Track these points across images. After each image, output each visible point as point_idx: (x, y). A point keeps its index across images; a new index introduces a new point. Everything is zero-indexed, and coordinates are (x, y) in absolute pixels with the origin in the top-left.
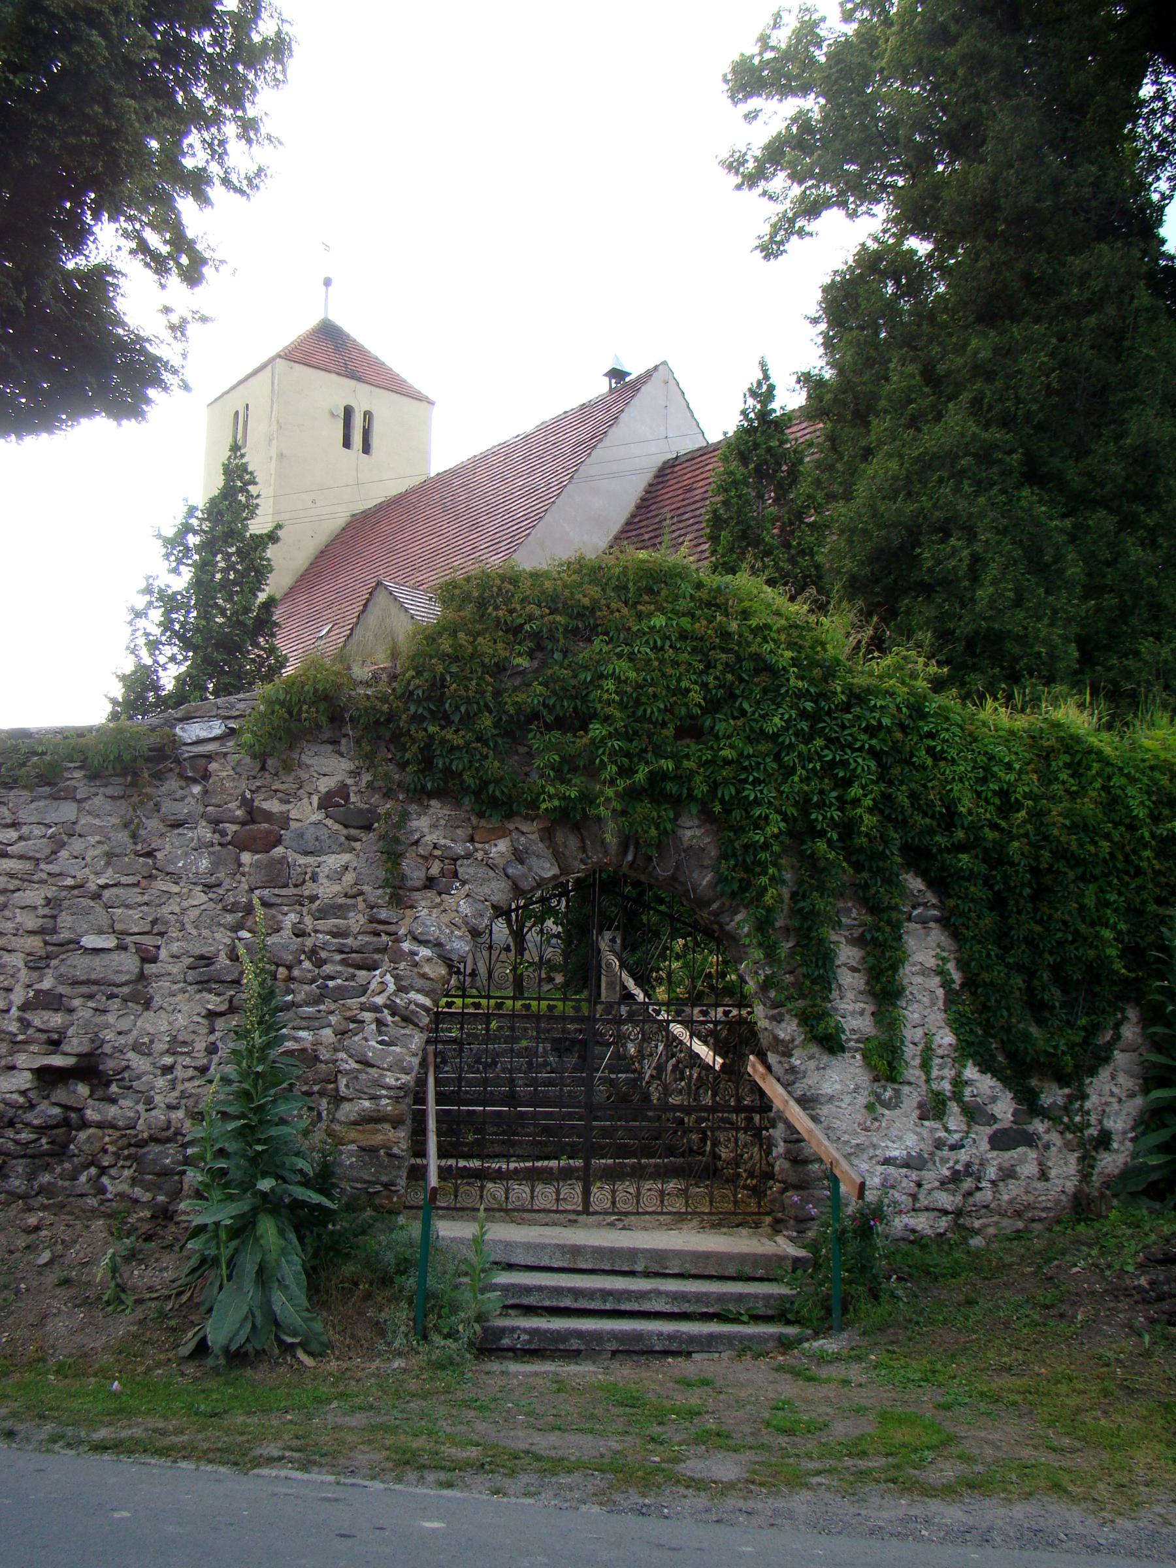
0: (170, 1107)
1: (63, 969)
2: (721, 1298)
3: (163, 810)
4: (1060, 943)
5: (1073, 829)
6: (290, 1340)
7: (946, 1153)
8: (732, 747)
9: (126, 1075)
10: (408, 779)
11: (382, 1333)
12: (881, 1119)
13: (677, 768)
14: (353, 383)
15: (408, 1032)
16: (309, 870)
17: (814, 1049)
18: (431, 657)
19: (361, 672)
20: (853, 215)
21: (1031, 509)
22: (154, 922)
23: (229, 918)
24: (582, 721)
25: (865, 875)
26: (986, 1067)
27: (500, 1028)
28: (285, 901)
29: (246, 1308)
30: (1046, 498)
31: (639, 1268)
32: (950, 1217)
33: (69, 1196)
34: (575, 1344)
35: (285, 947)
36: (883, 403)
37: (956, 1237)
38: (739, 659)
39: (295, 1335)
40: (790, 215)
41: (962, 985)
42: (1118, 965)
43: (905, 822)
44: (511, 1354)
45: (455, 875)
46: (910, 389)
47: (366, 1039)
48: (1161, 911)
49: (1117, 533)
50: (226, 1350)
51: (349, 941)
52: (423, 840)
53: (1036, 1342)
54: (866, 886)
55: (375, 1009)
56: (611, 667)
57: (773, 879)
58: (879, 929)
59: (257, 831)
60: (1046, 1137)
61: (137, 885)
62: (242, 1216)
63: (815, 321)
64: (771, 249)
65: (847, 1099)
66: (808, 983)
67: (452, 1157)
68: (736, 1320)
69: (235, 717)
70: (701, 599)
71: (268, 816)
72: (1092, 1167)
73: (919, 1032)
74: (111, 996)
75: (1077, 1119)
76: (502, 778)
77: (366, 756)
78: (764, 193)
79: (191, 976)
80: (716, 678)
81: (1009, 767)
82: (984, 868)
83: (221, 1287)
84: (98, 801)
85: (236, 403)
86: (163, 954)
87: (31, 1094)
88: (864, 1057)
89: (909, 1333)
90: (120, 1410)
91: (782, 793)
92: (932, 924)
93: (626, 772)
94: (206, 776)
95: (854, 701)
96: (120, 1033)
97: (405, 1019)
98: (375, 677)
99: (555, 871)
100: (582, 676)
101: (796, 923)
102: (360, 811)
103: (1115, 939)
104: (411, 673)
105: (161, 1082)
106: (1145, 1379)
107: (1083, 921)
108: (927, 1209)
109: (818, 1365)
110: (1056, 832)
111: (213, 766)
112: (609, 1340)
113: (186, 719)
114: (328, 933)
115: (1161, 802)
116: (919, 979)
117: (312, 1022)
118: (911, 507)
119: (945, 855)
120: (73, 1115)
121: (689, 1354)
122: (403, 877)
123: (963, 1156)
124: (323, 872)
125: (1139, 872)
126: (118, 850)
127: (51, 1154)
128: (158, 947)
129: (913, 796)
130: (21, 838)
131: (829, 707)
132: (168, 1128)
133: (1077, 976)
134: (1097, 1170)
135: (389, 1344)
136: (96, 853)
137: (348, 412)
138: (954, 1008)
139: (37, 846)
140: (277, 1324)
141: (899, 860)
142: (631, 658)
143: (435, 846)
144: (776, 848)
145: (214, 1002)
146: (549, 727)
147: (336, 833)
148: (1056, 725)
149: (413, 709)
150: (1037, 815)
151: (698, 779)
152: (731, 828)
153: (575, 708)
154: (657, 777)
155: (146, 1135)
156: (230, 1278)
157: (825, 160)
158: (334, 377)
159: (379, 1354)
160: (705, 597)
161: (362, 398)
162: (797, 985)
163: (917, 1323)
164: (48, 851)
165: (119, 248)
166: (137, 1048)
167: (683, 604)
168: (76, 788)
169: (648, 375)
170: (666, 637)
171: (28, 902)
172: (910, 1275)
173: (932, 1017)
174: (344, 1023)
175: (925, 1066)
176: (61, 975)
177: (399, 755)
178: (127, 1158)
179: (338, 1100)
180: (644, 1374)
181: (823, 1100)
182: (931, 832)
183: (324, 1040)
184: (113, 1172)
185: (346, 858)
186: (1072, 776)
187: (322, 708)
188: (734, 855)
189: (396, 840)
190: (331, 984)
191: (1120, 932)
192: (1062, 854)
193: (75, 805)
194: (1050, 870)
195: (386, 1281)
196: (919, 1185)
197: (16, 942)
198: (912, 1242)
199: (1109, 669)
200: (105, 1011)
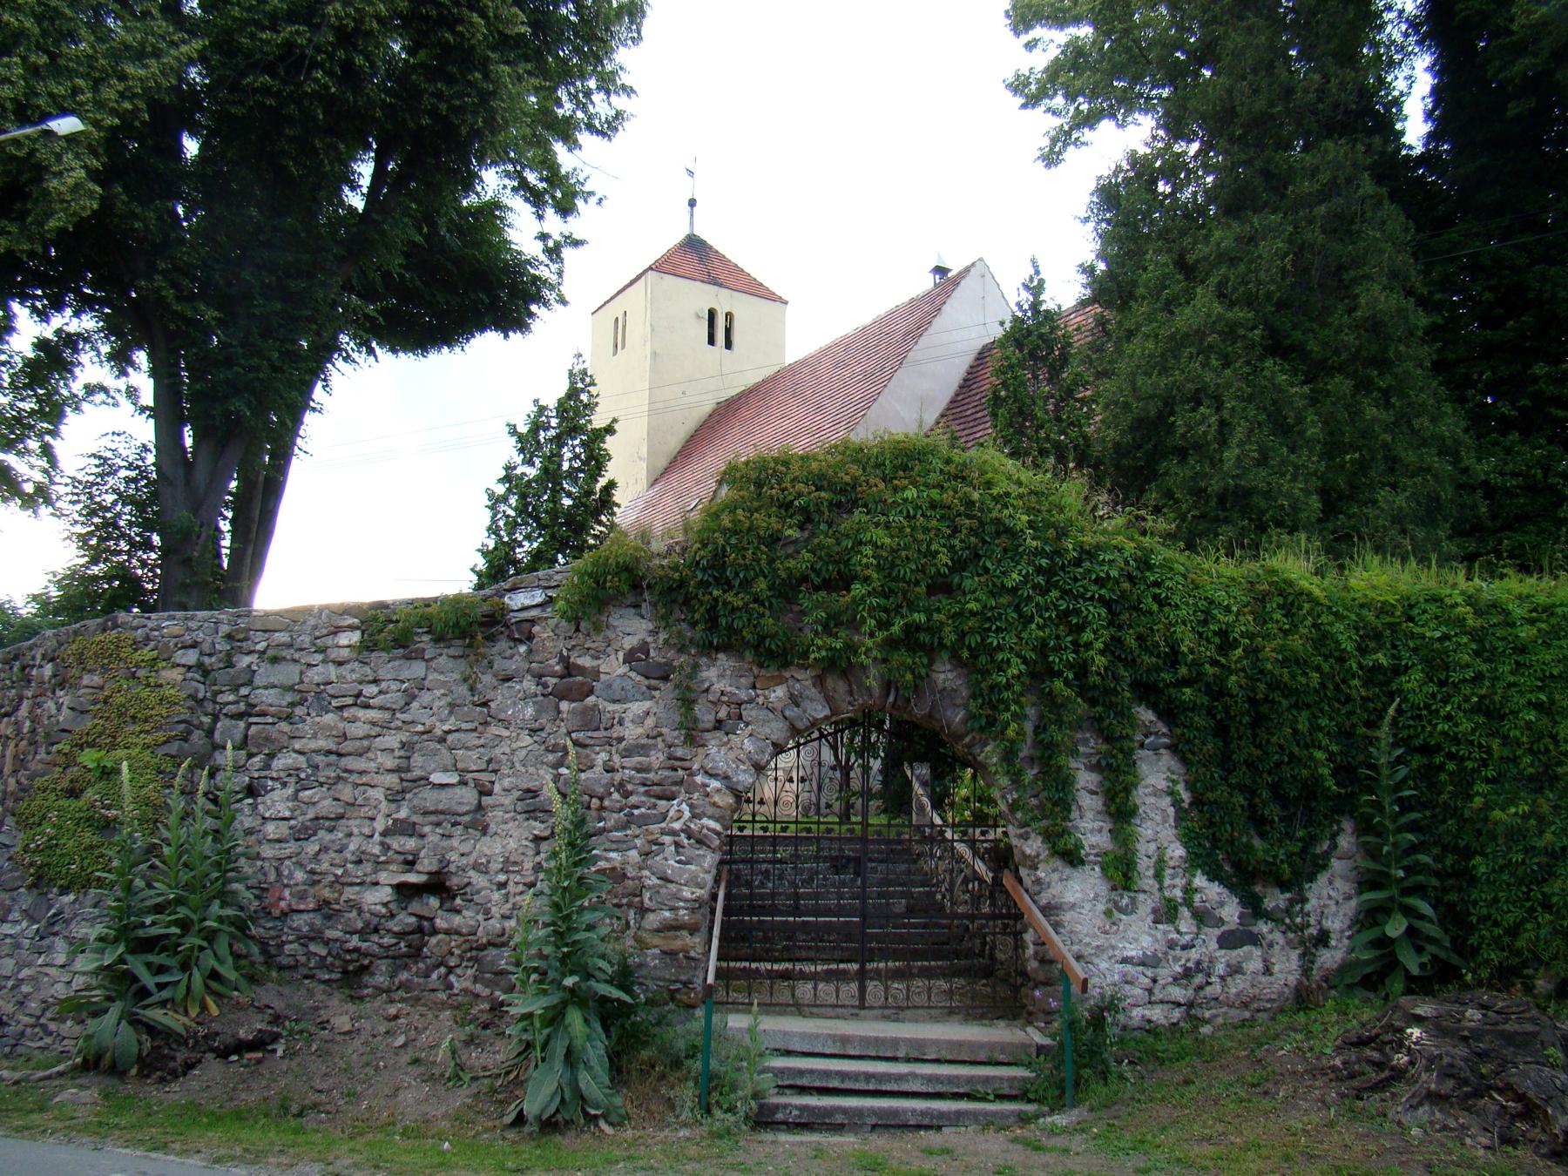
0: (504, 917)
1: (415, 802)
2: (970, 1080)
4: (1278, 765)
5: (1284, 663)
6: (593, 1112)
7: (1178, 952)
8: (977, 600)
10: (698, 636)
12: (1121, 921)
17: (1058, 863)
19: (657, 546)
20: (1121, 126)
21: (1273, 377)
22: (489, 762)
23: (551, 757)
24: (845, 582)
25: (1099, 709)
26: (1213, 876)
31: (901, 1054)
34: (839, 1119)
35: (598, 781)
36: (1141, 291)
38: (982, 524)
39: (597, 1108)
40: (1066, 128)
41: (1191, 804)
42: (1330, 783)
43: (1134, 661)
45: (740, 717)
46: (1165, 277)
48: (1369, 733)
49: (1353, 396)
50: (539, 1118)
51: (651, 775)
54: (1100, 719)
55: (674, 833)
57: (1015, 716)
58: (1114, 757)
59: (572, 683)
60: (1270, 937)
61: (475, 730)
62: (554, 1007)
64: (1051, 158)
65: (1088, 906)
66: (1049, 805)
68: (983, 1099)
71: (582, 670)
73: (1153, 846)
74: (454, 824)
75: (1298, 920)
77: (662, 618)
78: (1048, 110)
79: (520, 806)
81: (1228, 609)
82: (1205, 700)
86: (497, 788)
88: (1103, 869)
90: (441, 1164)
92: (1162, 751)
93: (883, 625)
94: (530, 637)
97: (699, 842)
98: (670, 549)
99: (827, 712)
100: (844, 544)
101: (1038, 753)
102: (659, 665)
104: (698, 545)
105: (496, 896)
106: (1325, 1146)
109: (1048, 1137)
110: (1269, 666)
111: (536, 629)
113: (513, 589)
115: (1368, 636)
116: (1152, 800)
117: (622, 846)
118: (1163, 381)
121: (939, 1128)
122: (696, 720)
123: (1194, 954)
124: (629, 716)
125: (1349, 699)
127: (409, 956)
128: (493, 783)
129: (1140, 638)
131: (1060, 566)
133: (1294, 793)
137: (712, 314)
140: (582, 1098)
141: (1128, 695)
142: (887, 526)
143: (722, 694)
144: (1017, 688)
145: (538, 828)
146: (817, 589)
148: (1273, 572)
150: (1253, 652)
151: (947, 629)
152: (979, 671)
153: (839, 572)
154: (911, 630)
156: (543, 1060)
158: (698, 284)
159: (669, 1125)
160: (953, 471)
161: (724, 301)
162: (1041, 807)
165: (505, 187)
166: (476, 867)
167: (934, 477)
169: (967, 270)
175: (1158, 876)
179: (643, 911)
180: (896, 1145)
182: (1158, 669)
184: (459, 971)
185: (647, 704)
186: (1285, 616)
188: (982, 695)
189: (688, 688)
190: (636, 812)
191: (1331, 754)
192: (1275, 685)
194: (1266, 700)
195: (677, 1064)
196: (1155, 981)
197: (378, 779)
199: (1350, 517)
200: (450, 836)
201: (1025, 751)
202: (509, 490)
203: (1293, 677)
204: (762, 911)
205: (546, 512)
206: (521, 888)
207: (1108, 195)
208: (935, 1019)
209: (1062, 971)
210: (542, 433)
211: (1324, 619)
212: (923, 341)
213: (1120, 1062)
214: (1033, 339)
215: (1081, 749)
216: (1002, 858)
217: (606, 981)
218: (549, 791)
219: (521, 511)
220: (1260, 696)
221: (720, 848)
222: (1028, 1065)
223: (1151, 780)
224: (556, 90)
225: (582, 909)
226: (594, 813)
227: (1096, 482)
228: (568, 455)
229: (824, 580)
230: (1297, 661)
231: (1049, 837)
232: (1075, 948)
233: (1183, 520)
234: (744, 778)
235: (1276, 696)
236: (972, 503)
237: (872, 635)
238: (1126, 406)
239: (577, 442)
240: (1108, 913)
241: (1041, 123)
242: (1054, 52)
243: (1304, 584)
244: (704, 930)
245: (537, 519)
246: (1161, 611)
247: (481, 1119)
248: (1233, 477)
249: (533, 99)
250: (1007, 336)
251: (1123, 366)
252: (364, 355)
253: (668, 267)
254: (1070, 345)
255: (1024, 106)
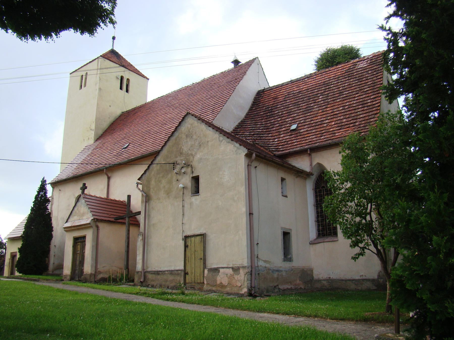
137: (122, 78)
161: (127, 74)
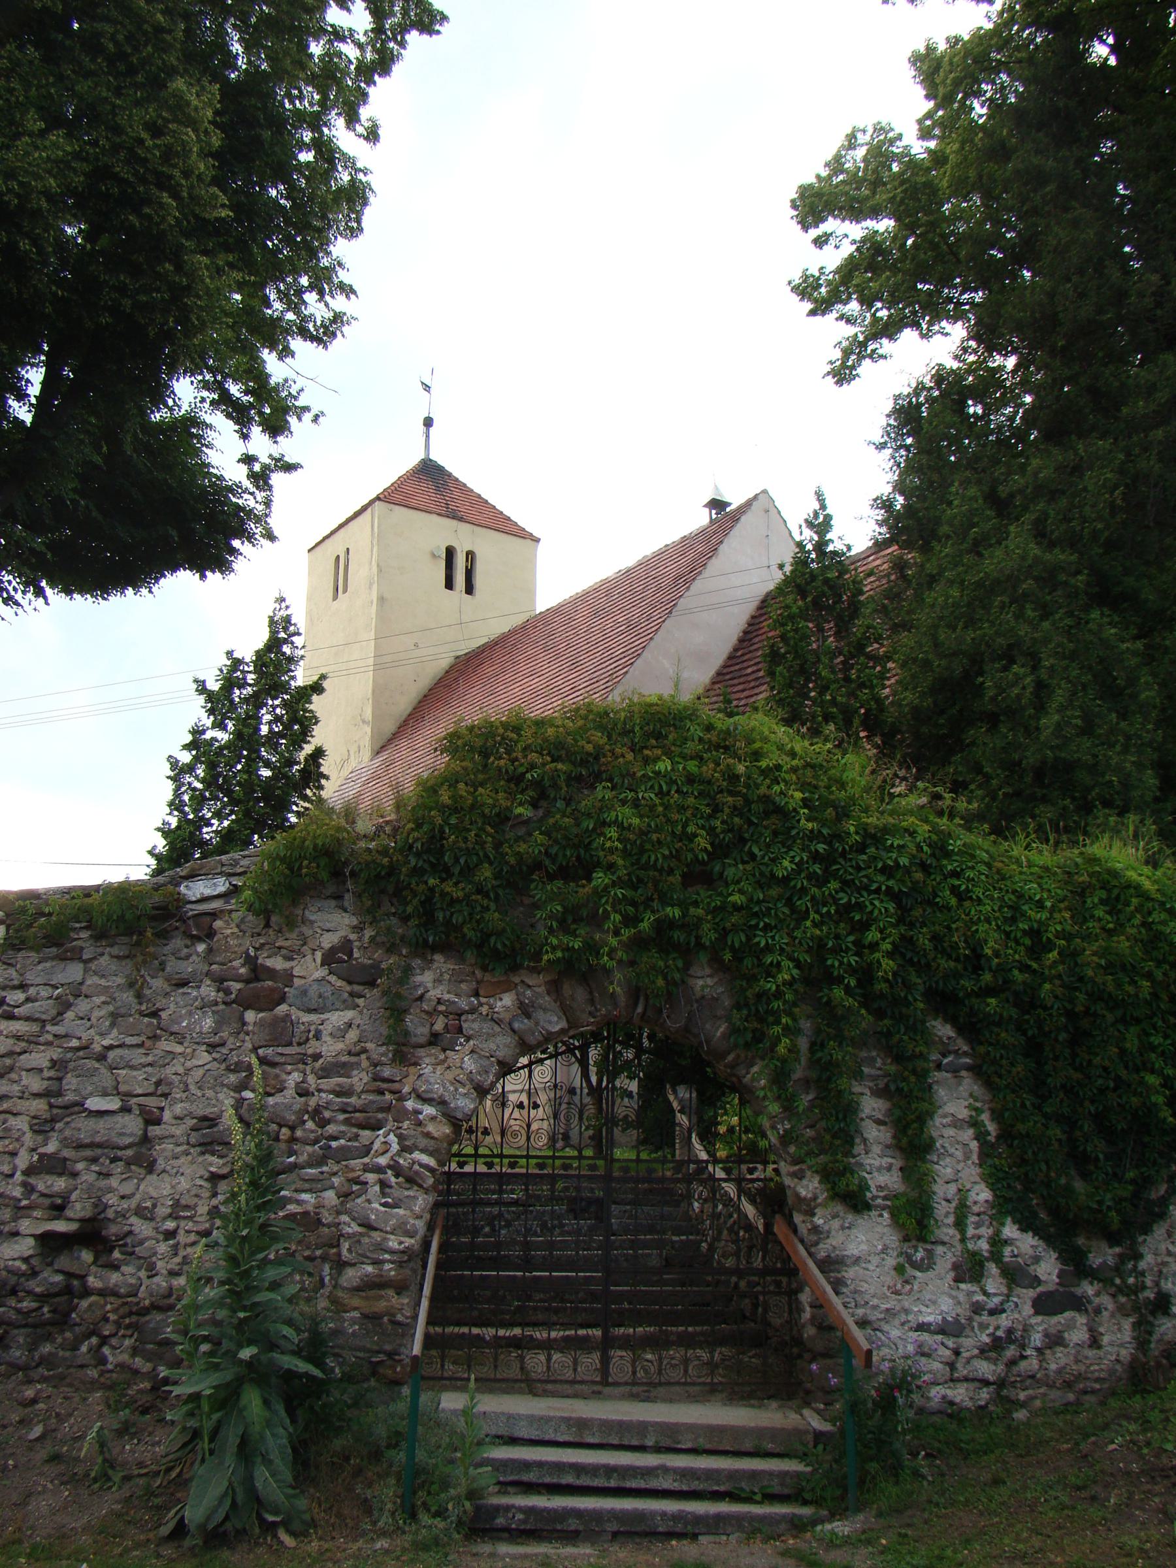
0: (173, 1274)
1: (67, 1133)
2: (732, 1475)
3: (168, 969)
4: (1102, 1091)
5: (1109, 968)
7: (985, 1318)
8: (741, 892)
9: (129, 1240)
10: (411, 932)
11: (369, 1511)
12: (914, 1285)
13: (684, 916)
14: (455, 522)
15: (411, 1193)
16: (313, 1028)
17: (839, 1208)
18: (431, 809)
19: (364, 826)
20: (925, 336)
22: (158, 1083)
23: (233, 1078)
24: (585, 869)
26: (1025, 1226)
27: (566, 1189)
28: (289, 1060)
29: (226, 1484)
30: (1117, 619)
31: (649, 1442)
32: (992, 1388)
33: (69, 1367)
34: (573, 1524)
35: (289, 1107)
36: (945, 529)
37: (999, 1410)
38: (748, 802)
39: (276, 1513)
40: (861, 338)
41: (998, 1137)
42: (1166, 1113)
43: (928, 965)
44: (506, 1535)
45: (460, 1030)
47: (369, 1201)
50: (202, 1527)
51: (353, 1100)
52: (428, 995)
53: (1059, 1527)
54: (889, 1035)
55: (379, 1169)
56: (613, 814)
57: (787, 1030)
58: (904, 1079)
59: (261, 989)
60: (1097, 1300)
61: (141, 1045)
62: (228, 1384)
63: (881, 447)
64: (843, 374)
65: (875, 1260)
66: (828, 1137)
67: (466, 1324)
68: (749, 1500)
69: (239, 874)
70: (710, 741)
71: (272, 973)
72: (1150, 1333)
73: (952, 1189)
75: (1131, 1280)
76: (504, 930)
77: (369, 912)
80: (723, 822)
81: (1040, 905)
83: (203, 1460)
84: (104, 961)
85: (336, 546)
86: (167, 1116)
87: (33, 1261)
88: (892, 1215)
89: (926, 1515)
91: (795, 938)
92: (964, 1073)
93: (630, 921)
94: (211, 934)
95: (869, 841)
96: (123, 1197)
98: (380, 829)
99: (563, 1024)
100: (584, 825)
103: (1162, 1086)
104: (411, 825)
105: (163, 1248)
107: (1126, 1067)
108: (966, 1379)
109: (826, 1550)
110: (1090, 973)
111: (218, 924)
112: (609, 1520)
113: (192, 876)
114: (331, 1092)
116: (950, 1132)
117: (316, 1185)
119: (973, 1000)
120: (75, 1283)
121: (694, 1537)
122: (407, 1033)
123: (1004, 1321)
124: (327, 1029)
126: (123, 1011)
128: (162, 1109)
129: (935, 938)
130: (28, 1000)
131: (841, 852)
132: (170, 1295)
134: (1155, 1337)
135: (374, 1523)
136: (102, 1013)
137: (450, 553)
138: (990, 1162)
139: (43, 1007)
140: (258, 1500)
141: (921, 1005)
142: (636, 804)
143: (439, 1001)
145: (215, 1164)
146: (551, 877)
147: (340, 989)
148: (1093, 860)
149: (413, 862)
150: (1070, 955)
151: (706, 926)
153: (578, 858)
155: (147, 1302)
156: (212, 1452)
157: (884, 288)
158: (434, 517)
159: (364, 1534)
161: (464, 537)
162: (818, 1139)
163: (937, 1505)
164: (54, 1012)
166: (140, 1212)
167: (691, 747)
168: (82, 949)
169: (748, 504)
170: (672, 782)
171: (34, 1064)
172: (939, 1451)
173: (967, 1171)
174: (346, 1185)
175: (960, 1224)
176: (65, 1139)
177: (401, 908)
178: (128, 1327)
179: (340, 1265)
181: (849, 1262)
182: (957, 975)
183: (326, 1202)
184: (114, 1341)
185: (349, 1014)
186: (1109, 913)
187: (322, 864)
188: (747, 1005)
189: (398, 996)
190: (334, 1144)
193: (81, 965)
194: (1087, 1012)
195: (376, 1455)
196: (957, 1353)
198: (950, 1416)
200: (108, 1175)
201: (798, 1074)
202: (196, 759)
203: (1119, 985)
204: (481, 1263)
205: (239, 784)
206: (193, 1237)
207: (906, 415)
208: (693, 1399)
209: (843, 1340)
210: (237, 692)
211: (1155, 917)
212: (697, 586)
213: (915, 1455)
214: (816, 585)
215: (866, 1070)
216: (775, 1201)
217: (293, 1353)
218: (229, 1118)
219: (209, 782)
220: (1079, 1008)
221: (434, 1187)
222: (803, 1457)
223: (950, 1108)
224: (264, 287)
225: (265, 1262)
226: (283, 1146)
227: (886, 752)
228: (267, 718)
229: (561, 868)
230: (1123, 967)
231: (829, 1176)
232: (860, 1312)
233: (994, 799)
234: (464, 1103)
235: (1099, 1008)
236: (738, 777)
237: (617, 933)
238: (926, 663)
239: (277, 702)
240: (899, 1269)
241: (832, 332)
242: (848, 249)
243: (1132, 875)
244: (414, 1288)
245: (229, 793)
246: (960, 905)
247: (132, 1531)
248: (1052, 748)
249: (238, 297)
250: (787, 581)
251: (923, 617)
252: (30, 596)
253: (398, 497)
254: (861, 593)
255: (812, 313)
